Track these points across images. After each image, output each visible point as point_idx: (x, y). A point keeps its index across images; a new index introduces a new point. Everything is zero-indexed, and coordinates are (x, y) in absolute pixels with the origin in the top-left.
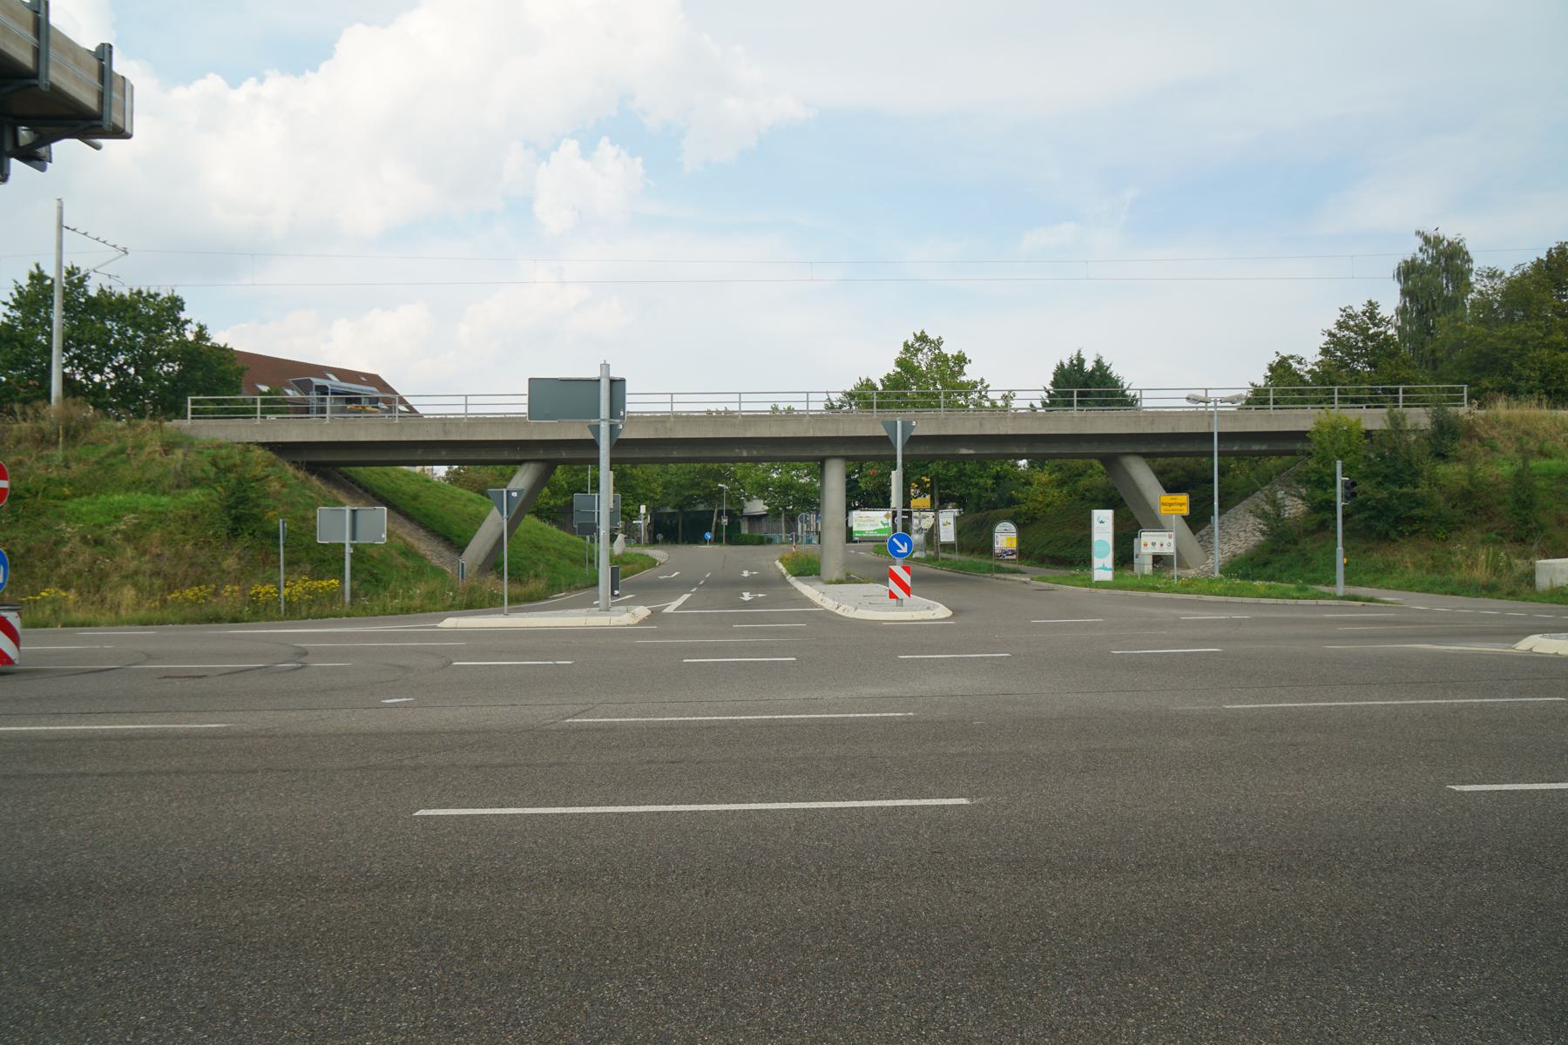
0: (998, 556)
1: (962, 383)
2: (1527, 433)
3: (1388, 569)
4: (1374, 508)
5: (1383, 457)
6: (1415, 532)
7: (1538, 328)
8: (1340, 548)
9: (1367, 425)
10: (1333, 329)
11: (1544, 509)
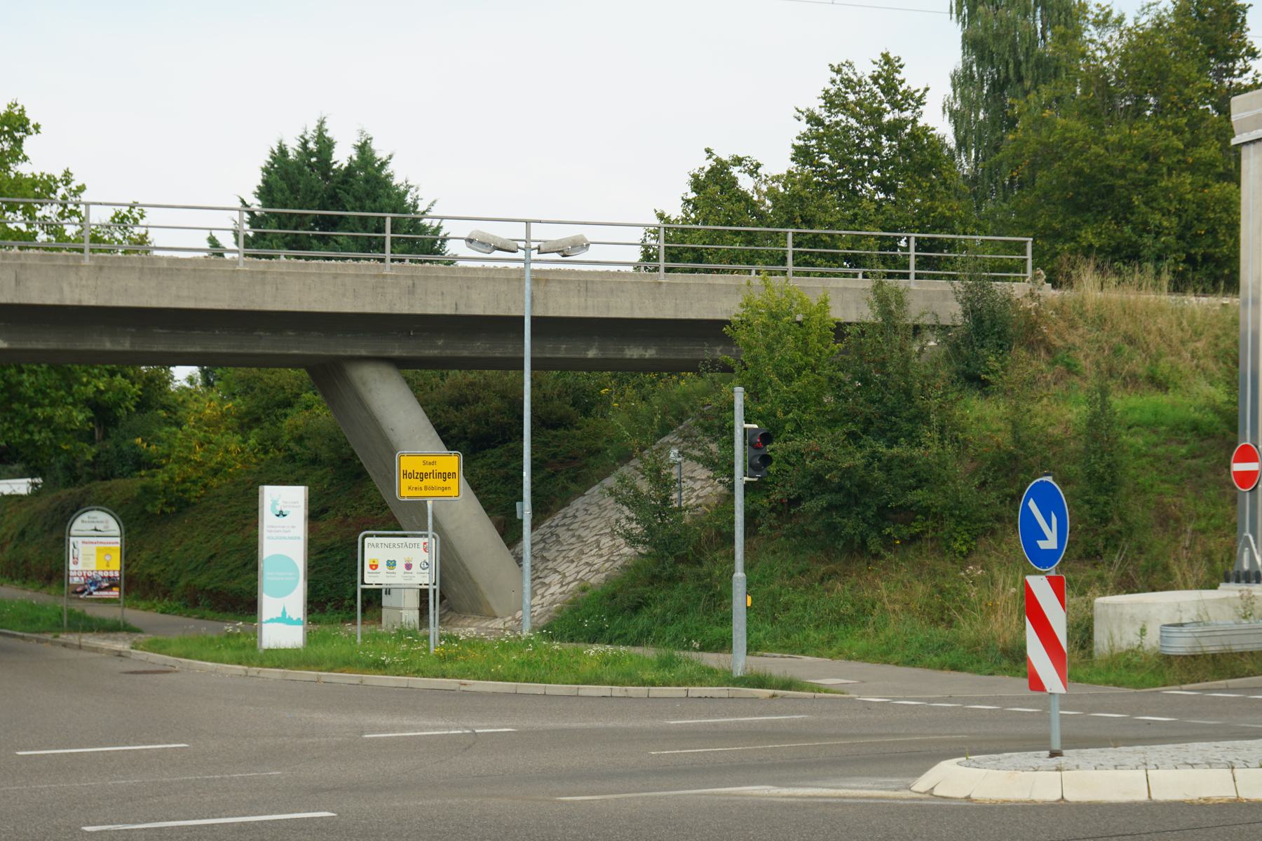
0: (78, 592)
1: (19, 180)
2: (1131, 341)
3: (861, 614)
4: (840, 488)
5: (866, 382)
6: (914, 538)
7: (1177, 131)
8: (739, 575)
9: (837, 313)
10: (817, 106)
11: (1140, 491)
